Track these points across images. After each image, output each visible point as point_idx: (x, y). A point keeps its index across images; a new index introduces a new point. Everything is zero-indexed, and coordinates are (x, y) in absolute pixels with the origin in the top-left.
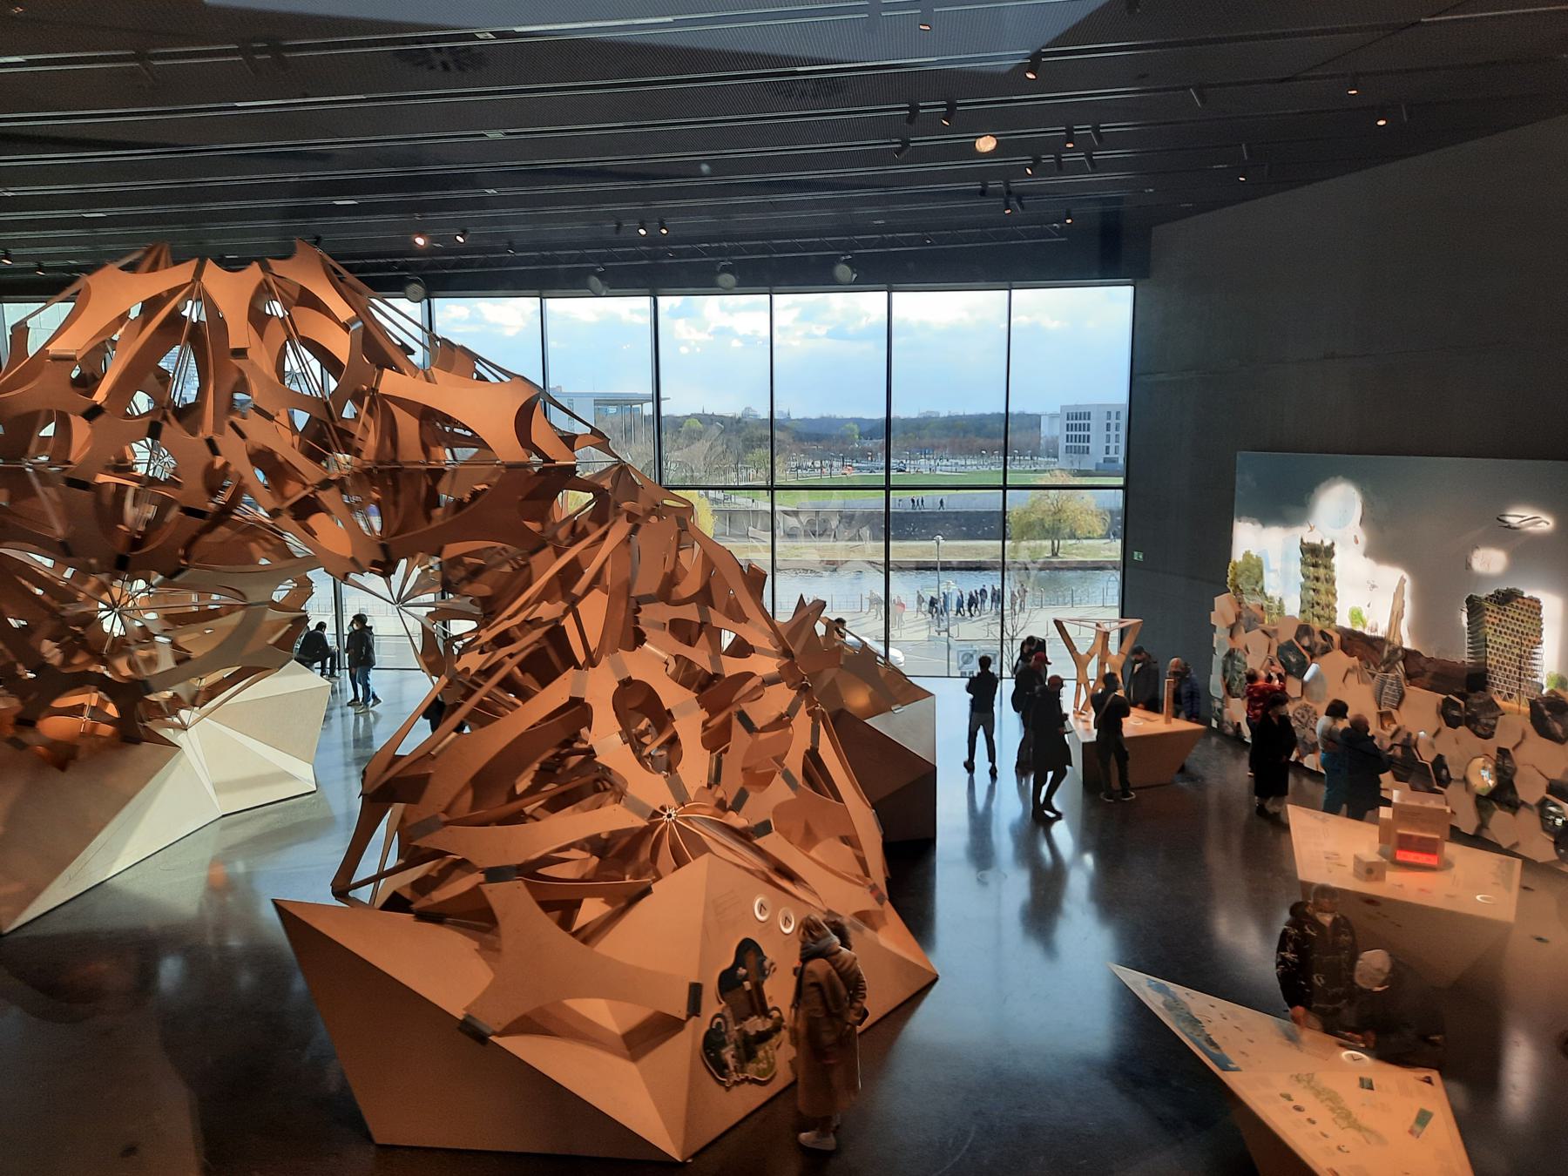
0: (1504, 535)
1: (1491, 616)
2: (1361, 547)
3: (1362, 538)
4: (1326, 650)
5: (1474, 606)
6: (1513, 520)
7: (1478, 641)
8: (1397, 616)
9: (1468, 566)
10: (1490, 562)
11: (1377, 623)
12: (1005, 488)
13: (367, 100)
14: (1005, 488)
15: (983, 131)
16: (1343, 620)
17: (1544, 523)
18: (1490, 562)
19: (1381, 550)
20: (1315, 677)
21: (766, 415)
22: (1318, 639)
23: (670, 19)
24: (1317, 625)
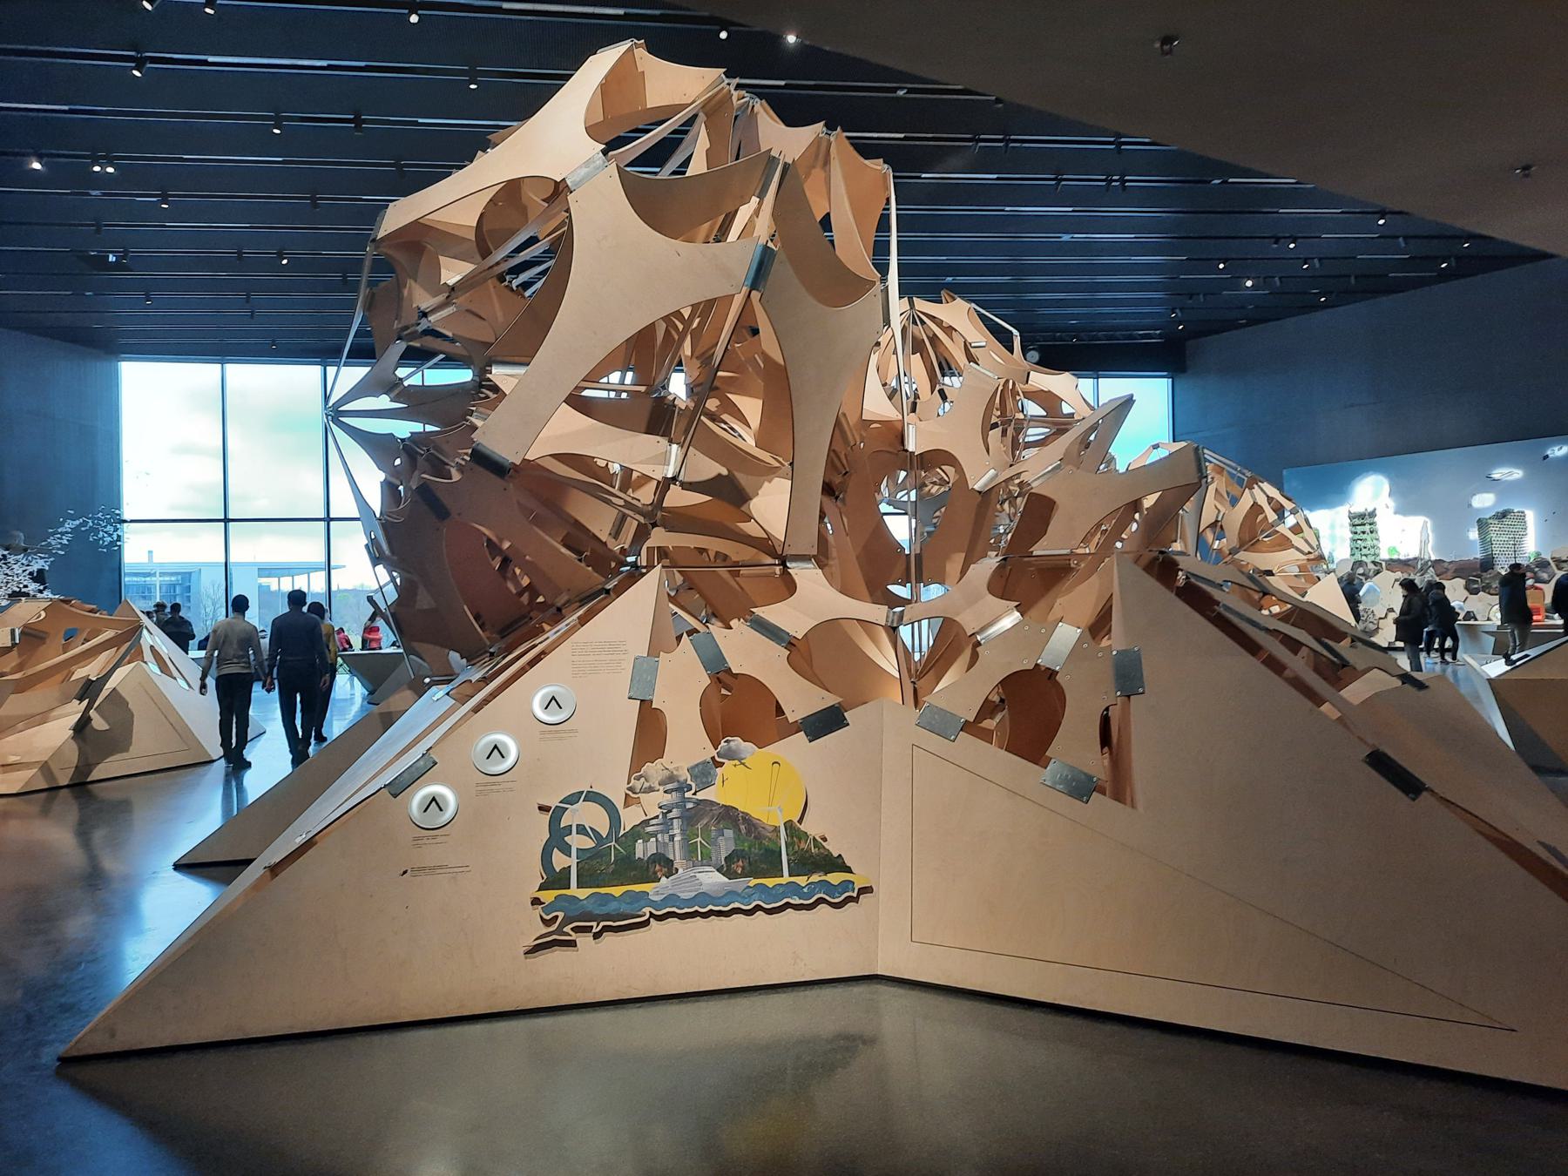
0: (1491, 484)
1: (1494, 528)
2: (1392, 510)
3: (1392, 504)
4: (1378, 572)
5: (1482, 525)
6: (1496, 476)
7: (1484, 539)
8: (1424, 543)
9: (1470, 505)
10: (1484, 501)
11: (1409, 550)
12: (226, 520)
13: (71, 111)
14: (226, 520)
15: (40, 158)
16: (1384, 555)
17: (1518, 474)
18: (1484, 501)
19: (1404, 509)
20: (1368, 591)
21: (126, 517)
22: (1371, 566)
23: (657, 12)
24: (1367, 560)
